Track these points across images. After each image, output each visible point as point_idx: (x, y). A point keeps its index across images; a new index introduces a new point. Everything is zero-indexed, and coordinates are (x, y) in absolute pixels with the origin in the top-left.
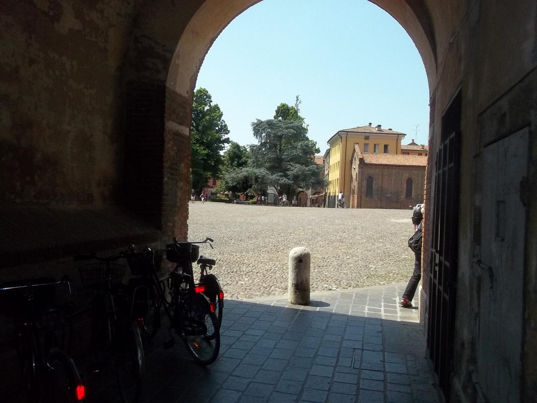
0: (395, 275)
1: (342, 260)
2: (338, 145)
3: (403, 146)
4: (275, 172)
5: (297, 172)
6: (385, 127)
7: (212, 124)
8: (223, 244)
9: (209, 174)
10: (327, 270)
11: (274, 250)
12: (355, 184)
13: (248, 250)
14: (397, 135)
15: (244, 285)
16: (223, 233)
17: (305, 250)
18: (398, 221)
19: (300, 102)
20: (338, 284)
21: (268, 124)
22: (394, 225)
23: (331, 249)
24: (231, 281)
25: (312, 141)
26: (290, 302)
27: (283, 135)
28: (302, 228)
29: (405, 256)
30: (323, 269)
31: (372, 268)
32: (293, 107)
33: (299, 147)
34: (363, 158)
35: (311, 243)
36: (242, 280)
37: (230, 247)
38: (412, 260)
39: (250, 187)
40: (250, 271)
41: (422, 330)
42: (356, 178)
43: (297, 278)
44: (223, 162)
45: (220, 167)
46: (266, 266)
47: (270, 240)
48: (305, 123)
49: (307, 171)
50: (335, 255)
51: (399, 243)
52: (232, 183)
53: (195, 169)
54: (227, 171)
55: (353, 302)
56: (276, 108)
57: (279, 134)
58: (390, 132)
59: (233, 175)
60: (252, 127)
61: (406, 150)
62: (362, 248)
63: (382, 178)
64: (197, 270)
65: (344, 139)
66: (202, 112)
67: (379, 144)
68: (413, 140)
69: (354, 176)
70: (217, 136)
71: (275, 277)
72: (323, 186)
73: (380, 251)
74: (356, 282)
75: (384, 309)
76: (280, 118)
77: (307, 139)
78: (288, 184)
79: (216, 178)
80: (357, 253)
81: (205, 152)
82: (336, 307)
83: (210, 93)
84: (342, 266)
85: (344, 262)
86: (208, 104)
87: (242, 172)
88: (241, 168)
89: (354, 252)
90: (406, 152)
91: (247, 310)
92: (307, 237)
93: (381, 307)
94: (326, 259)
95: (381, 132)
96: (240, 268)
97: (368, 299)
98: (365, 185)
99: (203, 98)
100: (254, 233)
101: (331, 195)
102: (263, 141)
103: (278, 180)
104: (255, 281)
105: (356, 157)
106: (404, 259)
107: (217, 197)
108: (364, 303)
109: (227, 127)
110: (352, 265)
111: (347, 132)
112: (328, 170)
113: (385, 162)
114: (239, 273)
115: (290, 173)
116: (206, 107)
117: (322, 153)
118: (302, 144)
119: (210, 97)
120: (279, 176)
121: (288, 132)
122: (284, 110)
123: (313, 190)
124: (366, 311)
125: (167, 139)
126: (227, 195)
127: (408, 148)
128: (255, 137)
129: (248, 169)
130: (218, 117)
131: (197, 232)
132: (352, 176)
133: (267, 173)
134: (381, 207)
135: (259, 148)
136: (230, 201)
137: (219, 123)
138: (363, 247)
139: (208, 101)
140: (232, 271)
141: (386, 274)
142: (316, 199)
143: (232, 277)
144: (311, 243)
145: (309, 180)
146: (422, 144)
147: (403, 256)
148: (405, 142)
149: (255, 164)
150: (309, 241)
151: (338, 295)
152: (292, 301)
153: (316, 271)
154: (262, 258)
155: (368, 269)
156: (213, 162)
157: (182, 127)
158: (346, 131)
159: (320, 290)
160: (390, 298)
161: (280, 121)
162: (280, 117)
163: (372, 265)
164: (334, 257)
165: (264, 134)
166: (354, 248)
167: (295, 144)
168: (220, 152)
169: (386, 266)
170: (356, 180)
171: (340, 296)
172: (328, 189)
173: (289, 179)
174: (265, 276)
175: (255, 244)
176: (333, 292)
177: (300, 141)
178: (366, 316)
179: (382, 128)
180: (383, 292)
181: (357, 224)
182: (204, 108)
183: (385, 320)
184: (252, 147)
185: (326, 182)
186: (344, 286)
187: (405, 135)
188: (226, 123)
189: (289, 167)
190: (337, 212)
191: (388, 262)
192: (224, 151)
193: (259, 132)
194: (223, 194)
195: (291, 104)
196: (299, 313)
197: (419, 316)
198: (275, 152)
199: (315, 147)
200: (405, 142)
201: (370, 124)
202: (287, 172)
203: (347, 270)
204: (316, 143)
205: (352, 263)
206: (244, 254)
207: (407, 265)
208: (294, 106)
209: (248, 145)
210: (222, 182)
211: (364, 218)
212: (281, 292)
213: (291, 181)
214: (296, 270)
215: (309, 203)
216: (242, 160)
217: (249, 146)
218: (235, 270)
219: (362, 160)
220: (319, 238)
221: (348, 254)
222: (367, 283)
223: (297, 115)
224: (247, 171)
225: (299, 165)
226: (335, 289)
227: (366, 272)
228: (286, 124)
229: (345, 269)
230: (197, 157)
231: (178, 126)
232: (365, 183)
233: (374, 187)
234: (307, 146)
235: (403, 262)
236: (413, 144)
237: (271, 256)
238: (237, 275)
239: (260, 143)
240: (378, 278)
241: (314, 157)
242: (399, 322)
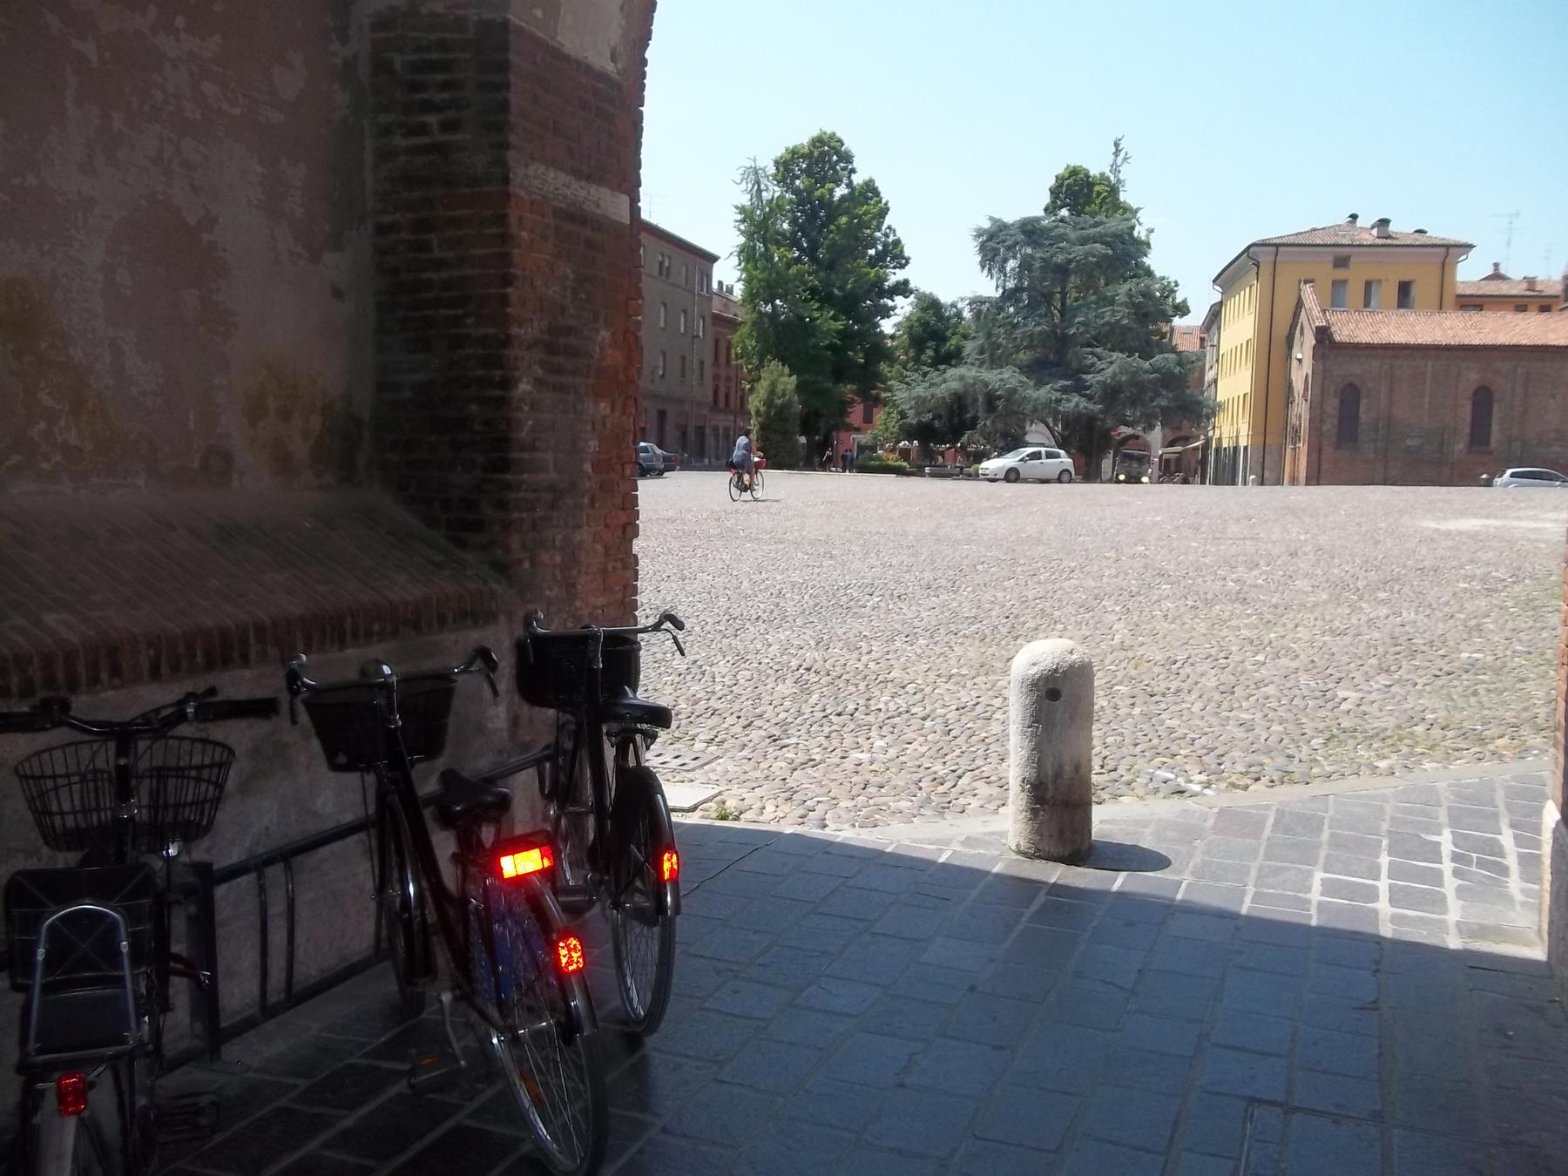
0: (1436, 732)
1: (1235, 669)
2: (1248, 290)
3: (1463, 283)
4: (1047, 379)
5: (1114, 375)
6: (1402, 226)
7: (856, 239)
8: (840, 610)
9: (848, 390)
10: (1178, 708)
11: (1004, 631)
12: (1301, 410)
13: (915, 631)
15: (866, 766)
16: (850, 572)
17: (1071, 652)
18: (1444, 526)
19: (1125, 159)
20: (1213, 766)
21: (1024, 232)
22: (1430, 540)
23: (1202, 627)
24: (826, 749)
25: (1163, 278)
26: (1014, 848)
27: (1069, 262)
28: (1112, 554)
29: (1475, 655)
30: (1163, 706)
31: (1346, 699)
32: (1102, 174)
33: (1122, 298)
34: (1329, 328)
35: (1136, 605)
36: (866, 745)
37: (860, 620)
38: (1500, 669)
39: (973, 425)
40: (901, 710)
41: (1559, 1002)
42: (1306, 389)
43: (1039, 758)
44: (892, 353)
45: (883, 367)
46: (963, 693)
47: (998, 594)
48: (1140, 224)
49: (1147, 372)
50: (1213, 652)
51: (1447, 603)
52: (918, 414)
53: (807, 377)
54: (902, 379)
55: (1262, 851)
56: (1052, 182)
57: (1060, 258)
58: (1421, 240)
59: (920, 390)
60: (976, 244)
61: (1472, 296)
62: (1312, 624)
63: (1391, 390)
64: (723, 706)
65: (1266, 270)
66: (826, 204)
67: (1380, 281)
68: (1496, 265)
69: (1298, 385)
70: (872, 275)
71: (985, 735)
72: (1199, 417)
73: (1376, 635)
74: (1281, 760)
75: (1390, 885)
76: (1064, 212)
77: (1149, 273)
78: (1086, 414)
79: (873, 404)
80: (1295, 643)
81: (839, 325)
82: (1192, 873)
83: (849, 145)
84: (1233, 693)
85: (1242, 678)
86: (845, 181)
87: (945, 381)
88: (942, 367)
89: (1283, 637)
90: (1472, 303)
91: (841, 880)
92: (1124, 585)
93: (1377, 878)
94: (1178, 665)
95: (1389, 241)
96: (869, 700)
97: (1325, 836)
99: (829, 160)
100: (951, 573)
101: (1225, 445)
102: (1011, 284)
103: (1058, 401)
104: (908, 752)
105: (1306, 324)
106: (1469, 664)
108: (1307, 855)
109: (903, 247)
110: (1271, 690)
111: (1275, 246)
112: (1215, 366)
114: (863, 717)
115: (1094, 381)
116: (837, 189)
117: (1196, 318)
118: (1130, 290)
119: (847, 158)
120: (1059, 391)
121: (1087, 255)
122: (1078, 185)
123: (1168, 431)
124: (1315, 895)
125: (524, 234)
126: (905, 454)
127: (1480, 288)
128: (986, 271)
129: (961, 371)
130: (873, 218)
131: (770, 568)
132: (1290, 383)
133: (1021, 382)
134: (1386, 481)
135: (998, 305)
136: (918, 472)
137: (878, 234)
138: (1316, 620)
139: (844, 169)
140: (839, 709)
141: (1399, 727)
142: (1178, 460)
143: (833, 735)
144: (1136, 605)
145: (1153, 401)
146: (1530, 275)
147: (1465, 655)
148: (1469, 273)
149: (986, 355)
150: (1128, 598)
151: (1205, 820)
152: (1022, 843)
153: (1137, 711)
154: (952, 662)
155: (1330, 705)
156: (861, 355)
157: (593, 189)
158: (1275, 241)
159: (1140, 792)
160: (1416, 835)
161: (1062, 220)
162: (1062, 207)
163: (1348, 689)
164: (1211, 656)
165: (1011, 261)
166: (1284, 625)
168: (881, 322)
169: (1402, 692)
171: (1215, 822)
172: (1214, 428)
173: (1090, 398)
174: (950, 730)
175: (945, 609)
176: (1189, 801)
177: (1125, 281)
178: (1314, 923)
179: (1392, 228)
180: (1388, 809)
181: (1302, 538)
182: (831, 191)
183: (1396, 943)
184: (977, 302)
185: (1208, 407)
186: (1233, 779)
187: (1471, 247)
189: (1091, 359)
190: (1244, 497)
191: (1409, 677)
192: (894, 320)
193: (996, 255)
194: (893, 450)
195: (1097, 166)
196: (1041, 898)
197: (1540, 921)
198: (1046, 315)
199: (1174, 299)
200: (1469, 273)
202: (1084, 376)
203: (1252, 711)
204: (1177, 286)
205: (1272, 683)
206: (898, 644)
207: (1481, 688)
208: (1108, 173)
209: (962, 299)
210: (889, 413)
211: (1326, 516)
212: (990, 799)
213: (1095, 403)
214: (1038, 728)
215: (1153, 470)
216: (948, 344)
217: (967, 302)
218: (851, 707)
219: (1323, 334)
220: (1164, 587)
221: (1260, 647)
222: (1325, 763)
223: (1118, 199)
224: (962, 378)
225: (1120, 355)
226: (1197, 788)
227: (1323, 719)
228: (1082, 229)
229: (1245, 704)
230: (814, 340)
231: (575, 185)
232: (1332, 405)
233: (1363, 417)
234: (1147, 294)
235: (1465, 676)
236: (1497, 276)
237: (990, 651)
238: (852, 727)
239: (1000, 291)
240: (1368, 742)
241: (1172, 330)
242: (1454, 951)
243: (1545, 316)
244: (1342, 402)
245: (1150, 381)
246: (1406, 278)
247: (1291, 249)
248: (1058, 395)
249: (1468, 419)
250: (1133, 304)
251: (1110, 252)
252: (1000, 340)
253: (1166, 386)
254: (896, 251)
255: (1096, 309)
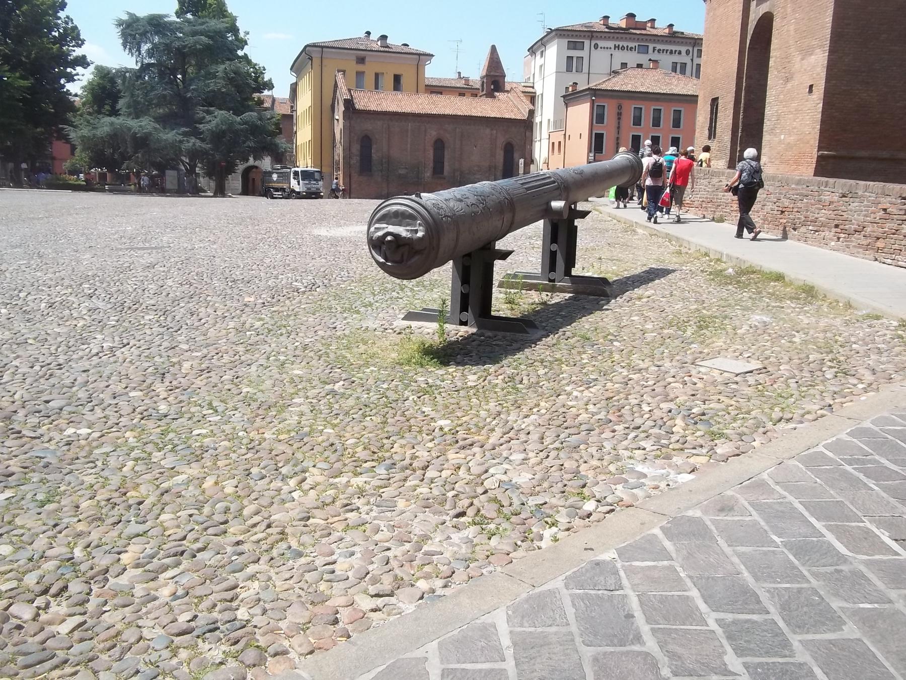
5: (218, 125)
6: (394, 41)
14: (417, 57)
25: (256, 64)
27: (185, 47)
49: (239, 124)
58: (405, 50)
65: (316, 61)
76: (189, 16)
90: (436, 90)
98: (358, 153)
103: (181, 142)
105: (339, 97)
107: (59, 180)
113: (393, 108)
117: (281, 92)
118: (226, 69)
121: (196, 42)
128: (127, 51)
133: (155, 128)
148: (433, 72)
167: (213, 68)
170: (340, 142)
173: (203, 140)
179: (389, 41)
188: (75, 23)
199: (263, 78)
201: (368, 33)
202: (197, 125)
219: (349, 104)
224: (112, 124)
232: (356, 148)
239: (139, 64)
243: (461, 98)
244: (362, 147)
245: (242, 130)
246: (397, 73)
247: (334, 50)
248: (180, 137)
249: (502, 160)
250: (229, 79)
251: (211, 42)
252: (139, 99)
253: (253, 134)
254: (74, 34)
255: (204, 81)
